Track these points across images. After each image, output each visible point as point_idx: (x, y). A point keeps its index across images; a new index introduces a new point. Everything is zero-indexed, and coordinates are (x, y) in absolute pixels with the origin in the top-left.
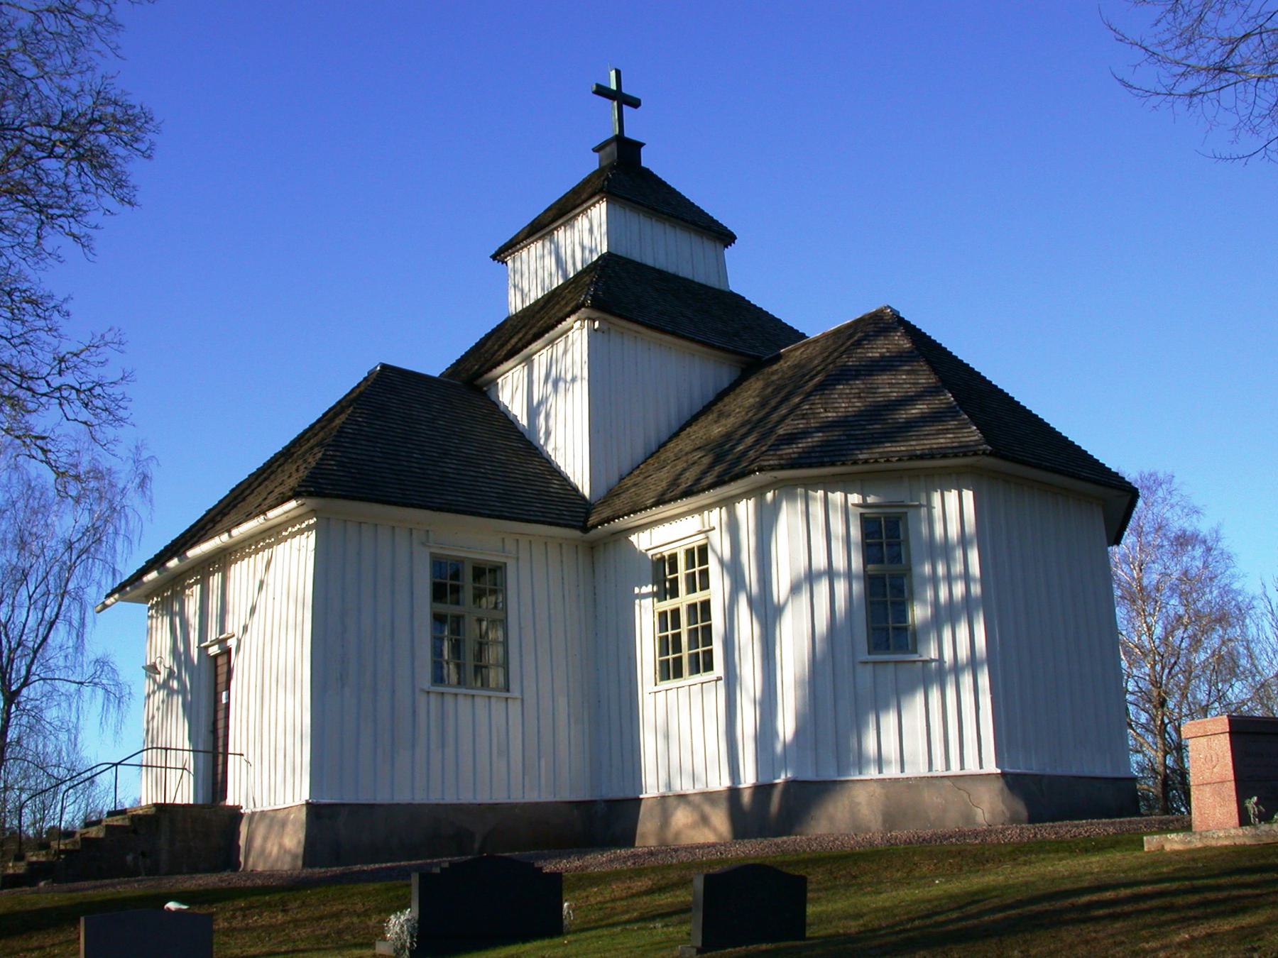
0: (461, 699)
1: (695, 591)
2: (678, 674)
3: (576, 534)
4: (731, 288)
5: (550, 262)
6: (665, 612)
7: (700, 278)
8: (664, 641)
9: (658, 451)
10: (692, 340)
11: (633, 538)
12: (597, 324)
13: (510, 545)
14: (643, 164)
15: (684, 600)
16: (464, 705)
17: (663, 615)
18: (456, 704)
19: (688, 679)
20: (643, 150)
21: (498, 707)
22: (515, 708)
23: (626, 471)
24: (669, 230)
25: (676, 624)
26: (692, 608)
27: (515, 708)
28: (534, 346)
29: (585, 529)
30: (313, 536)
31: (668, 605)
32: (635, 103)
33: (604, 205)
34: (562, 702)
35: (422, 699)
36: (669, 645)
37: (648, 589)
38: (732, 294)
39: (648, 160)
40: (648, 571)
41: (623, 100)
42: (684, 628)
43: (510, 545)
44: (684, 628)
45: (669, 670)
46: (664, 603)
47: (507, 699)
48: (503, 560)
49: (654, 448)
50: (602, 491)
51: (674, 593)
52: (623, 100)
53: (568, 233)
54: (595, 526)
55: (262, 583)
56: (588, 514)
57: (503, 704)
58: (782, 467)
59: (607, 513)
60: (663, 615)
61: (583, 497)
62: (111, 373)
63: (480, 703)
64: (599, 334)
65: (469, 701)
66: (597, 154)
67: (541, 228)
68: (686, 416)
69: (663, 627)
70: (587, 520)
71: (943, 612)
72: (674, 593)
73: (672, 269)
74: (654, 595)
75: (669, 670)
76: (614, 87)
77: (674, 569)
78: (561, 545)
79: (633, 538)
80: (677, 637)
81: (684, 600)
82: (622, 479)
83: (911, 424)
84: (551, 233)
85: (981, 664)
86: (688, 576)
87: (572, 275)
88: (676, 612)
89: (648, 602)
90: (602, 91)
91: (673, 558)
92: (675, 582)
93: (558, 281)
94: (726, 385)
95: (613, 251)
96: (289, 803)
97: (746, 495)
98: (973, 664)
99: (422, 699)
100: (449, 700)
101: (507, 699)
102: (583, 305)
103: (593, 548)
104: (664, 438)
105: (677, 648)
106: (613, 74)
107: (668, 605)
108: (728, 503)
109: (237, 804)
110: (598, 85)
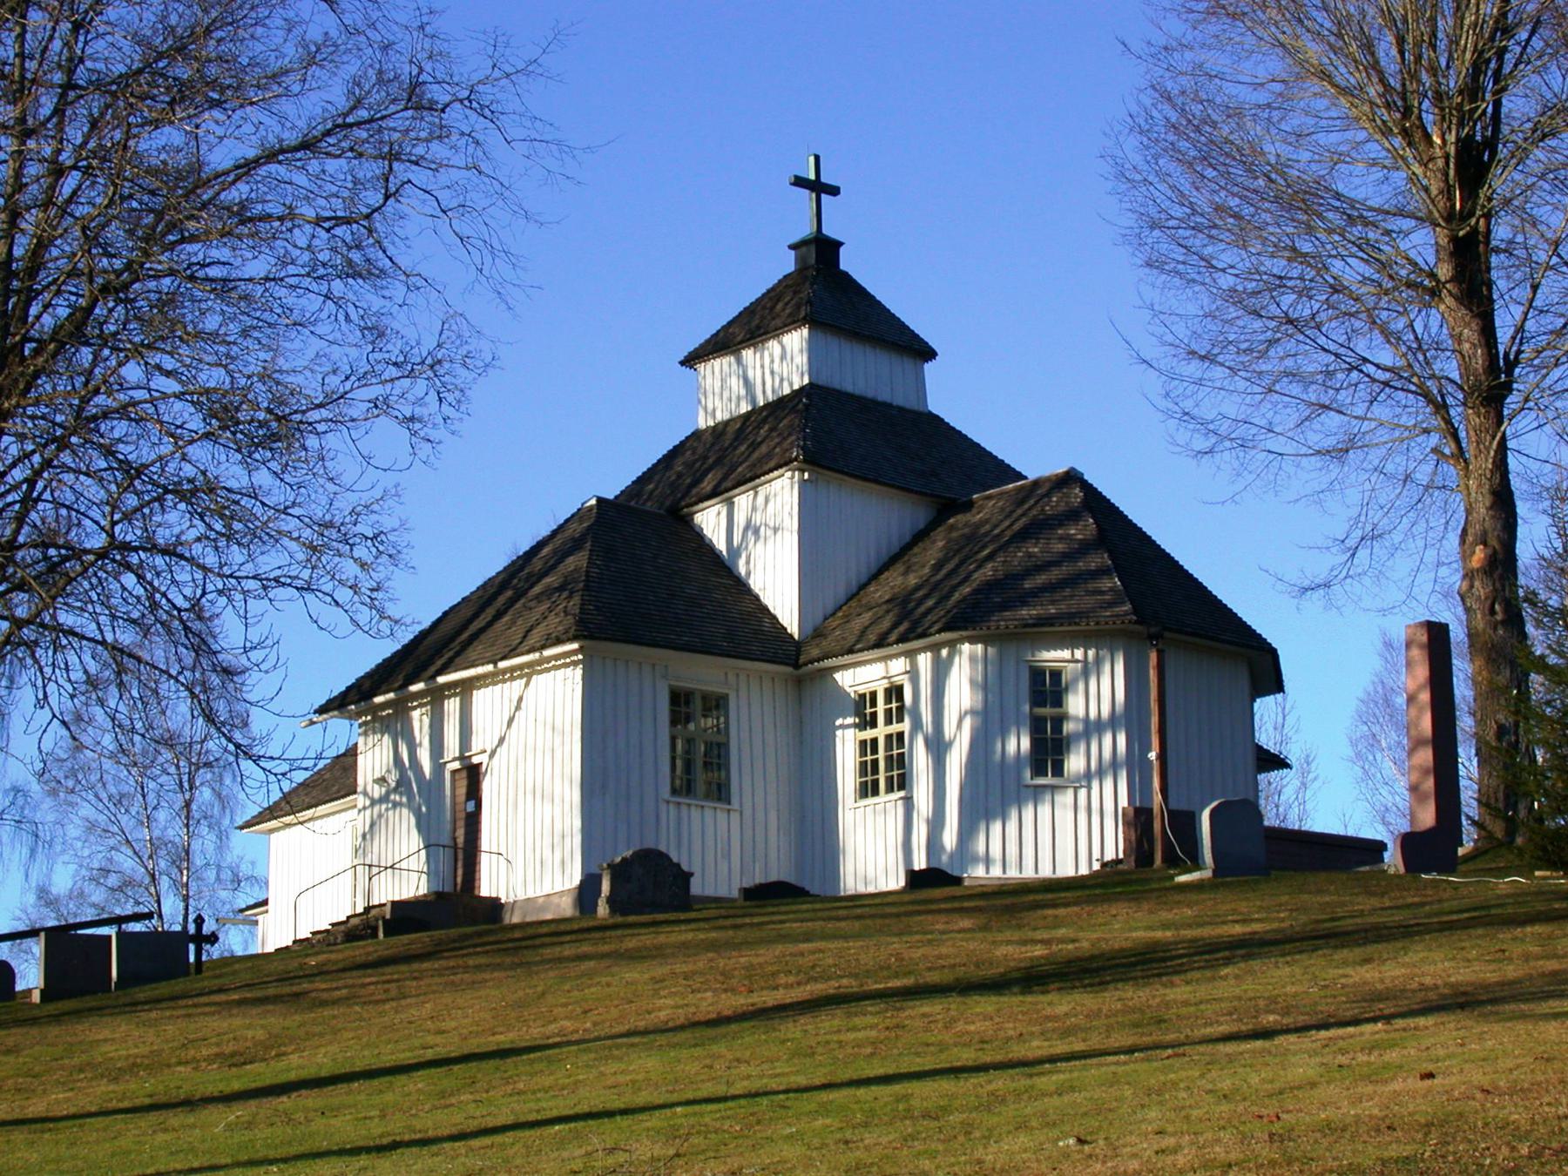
0: (693, 808)
1: (891, 723)
2: (875, 792)
3: (789, 669)
4: (930, 408)
5: (736, 384)
6: (865, 741)
7: (899, 401)
8: (863, 765)
9: (857, 593)
10: (893, 486)
11: (838, 676)
12: (806, 475)
13: (732, 678)
14: (842, 267)
15: (881, 731)
16: (695, 813)
17: (863, 743)
18: (679, 812)
19: (883, 797)
20: (842, 250)
21: (721, 816)
22: (735, 817)
23: (830, 611)
24: (868, 350)
25: (875, 750)
26: (889, 737)
27: (735, 817)
28: (737, 491)
29: (797, 666)
30: (579, 671)
31: (868, 734)
32: (834, 191)
33: (805, 331)
34: (773, 816)
35: (663, 807)
36: (867, 768)
37: (850, 720)
38: (930, 413)
39: (848, 262)
40: (852, 708)
41: (819, 188)
42: (881, 754)
43: (732, 678)
44: (881, 754)
45: (868, 789)
46: (864, 733)
47: (729, 811)
48: (726, 691)
49: (854, 590)
50: (809, 631)
51: (874, 724)
52: (819, 188)
53: (758, 355)
54: (806, 664)
55: (518, 708)
56: (798, 653)
57: (726, 815)
58: (307, 993)
59: (815, 652)
60: (863, 743)
61: (791, 636)
62: (388, 523)
63: (708, 813)
64: (808, 484)
65: (699, 810)
66: (793, 252)
67: (725, 342)
68: (885, 558)
69: (863, 753)
70: (798, 659)
71: (1092, 727)
72: (874, 724)
73: (870, 394)
74: (855, 726)
75: (868, 789)
76: (812, 176)
77: (874, 703)
78: (773, 679)
79: (838, 676)
80: (875, 763)
81: (881, 731)
82: (826, 619)
83: (1036, 593)
84: (739, 350)
85: (1121, 766)
86: (886, 710)
87: (762, 404)
88: (875, 741)
89: (850, 732)
90: (800, 182)
91: (874, 695)
92: (874, 715)
93: (745, 408)
94: (922, 526)
95: (814, 381)
96: (558, 888)
97: (924, 649)
98: (1114, 765)
99: (663, 807)
100: (684, 809)
101: (729, 811)
102: (796, 459)
103: (799, 682)
104: (864, 579)
105: (875, 770)
106: (812, 159)
107: (868, 734)
108: (911, 655)
109: (494, 895)
110: (796, 177)
